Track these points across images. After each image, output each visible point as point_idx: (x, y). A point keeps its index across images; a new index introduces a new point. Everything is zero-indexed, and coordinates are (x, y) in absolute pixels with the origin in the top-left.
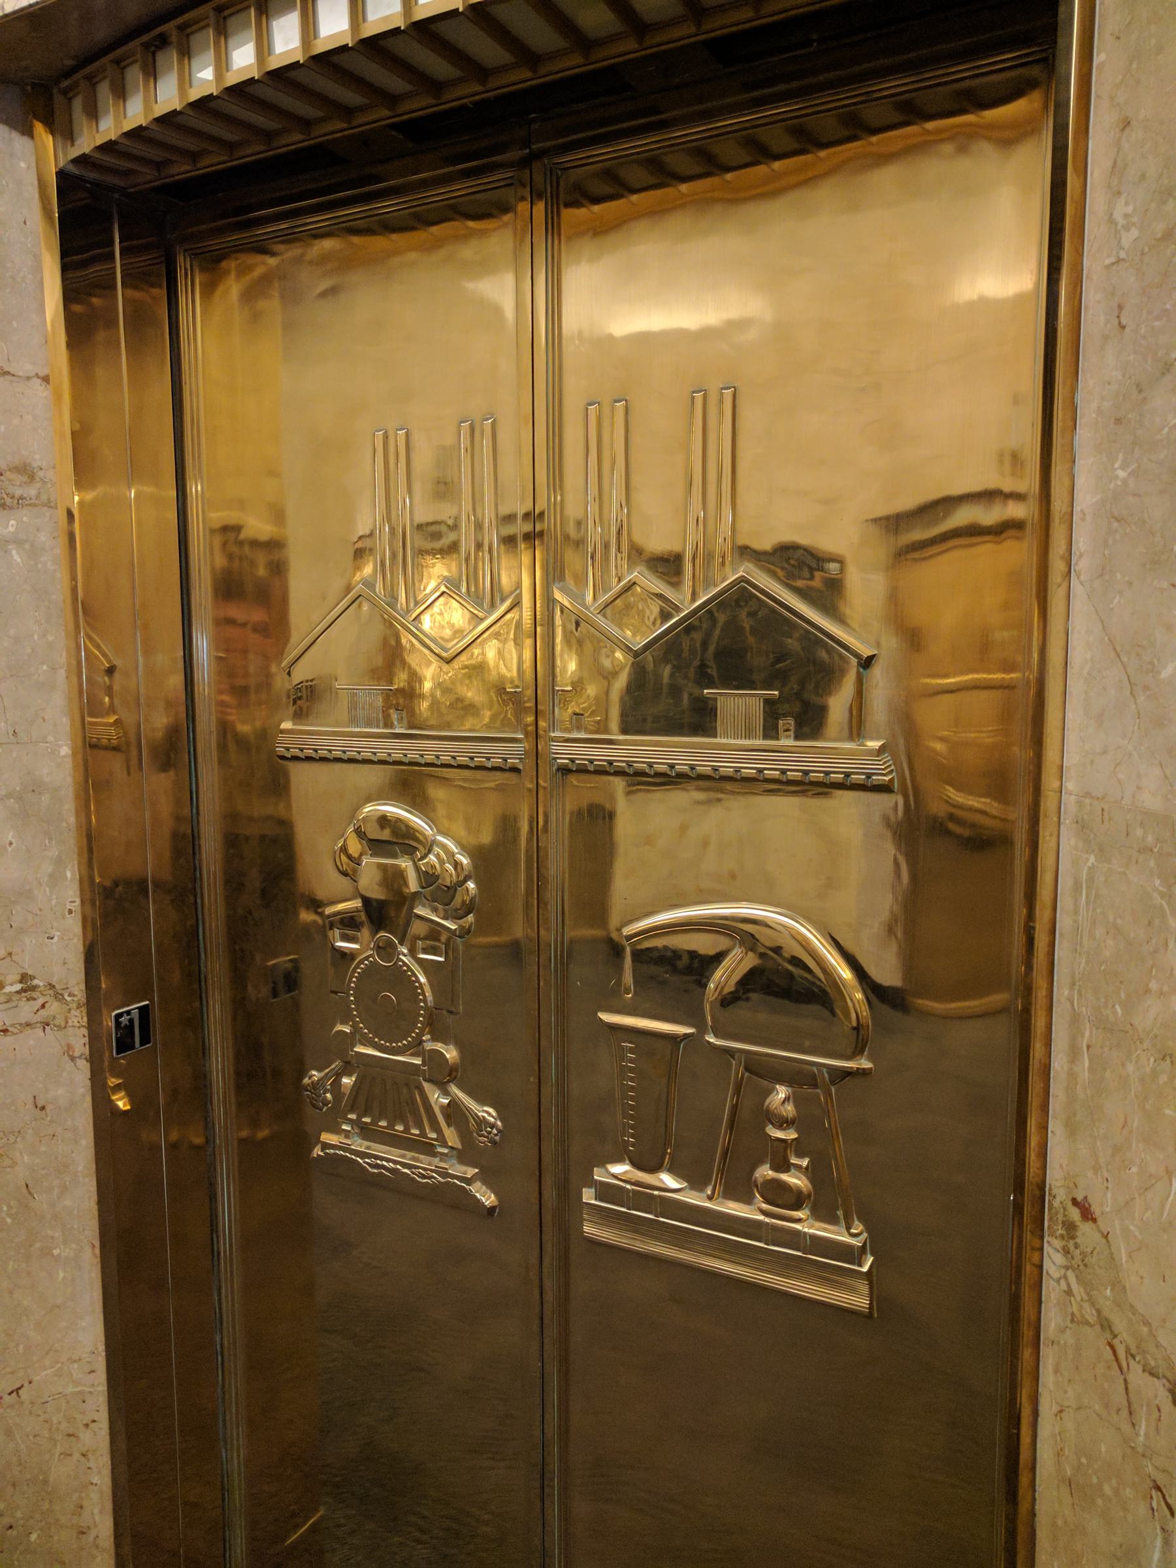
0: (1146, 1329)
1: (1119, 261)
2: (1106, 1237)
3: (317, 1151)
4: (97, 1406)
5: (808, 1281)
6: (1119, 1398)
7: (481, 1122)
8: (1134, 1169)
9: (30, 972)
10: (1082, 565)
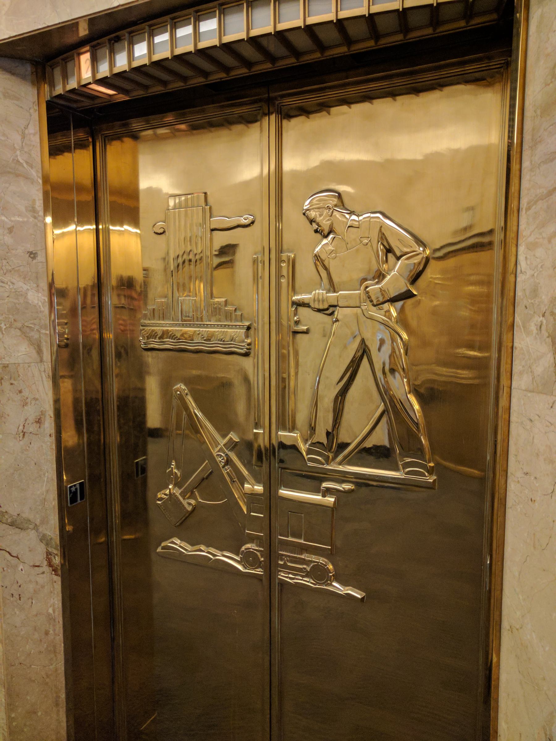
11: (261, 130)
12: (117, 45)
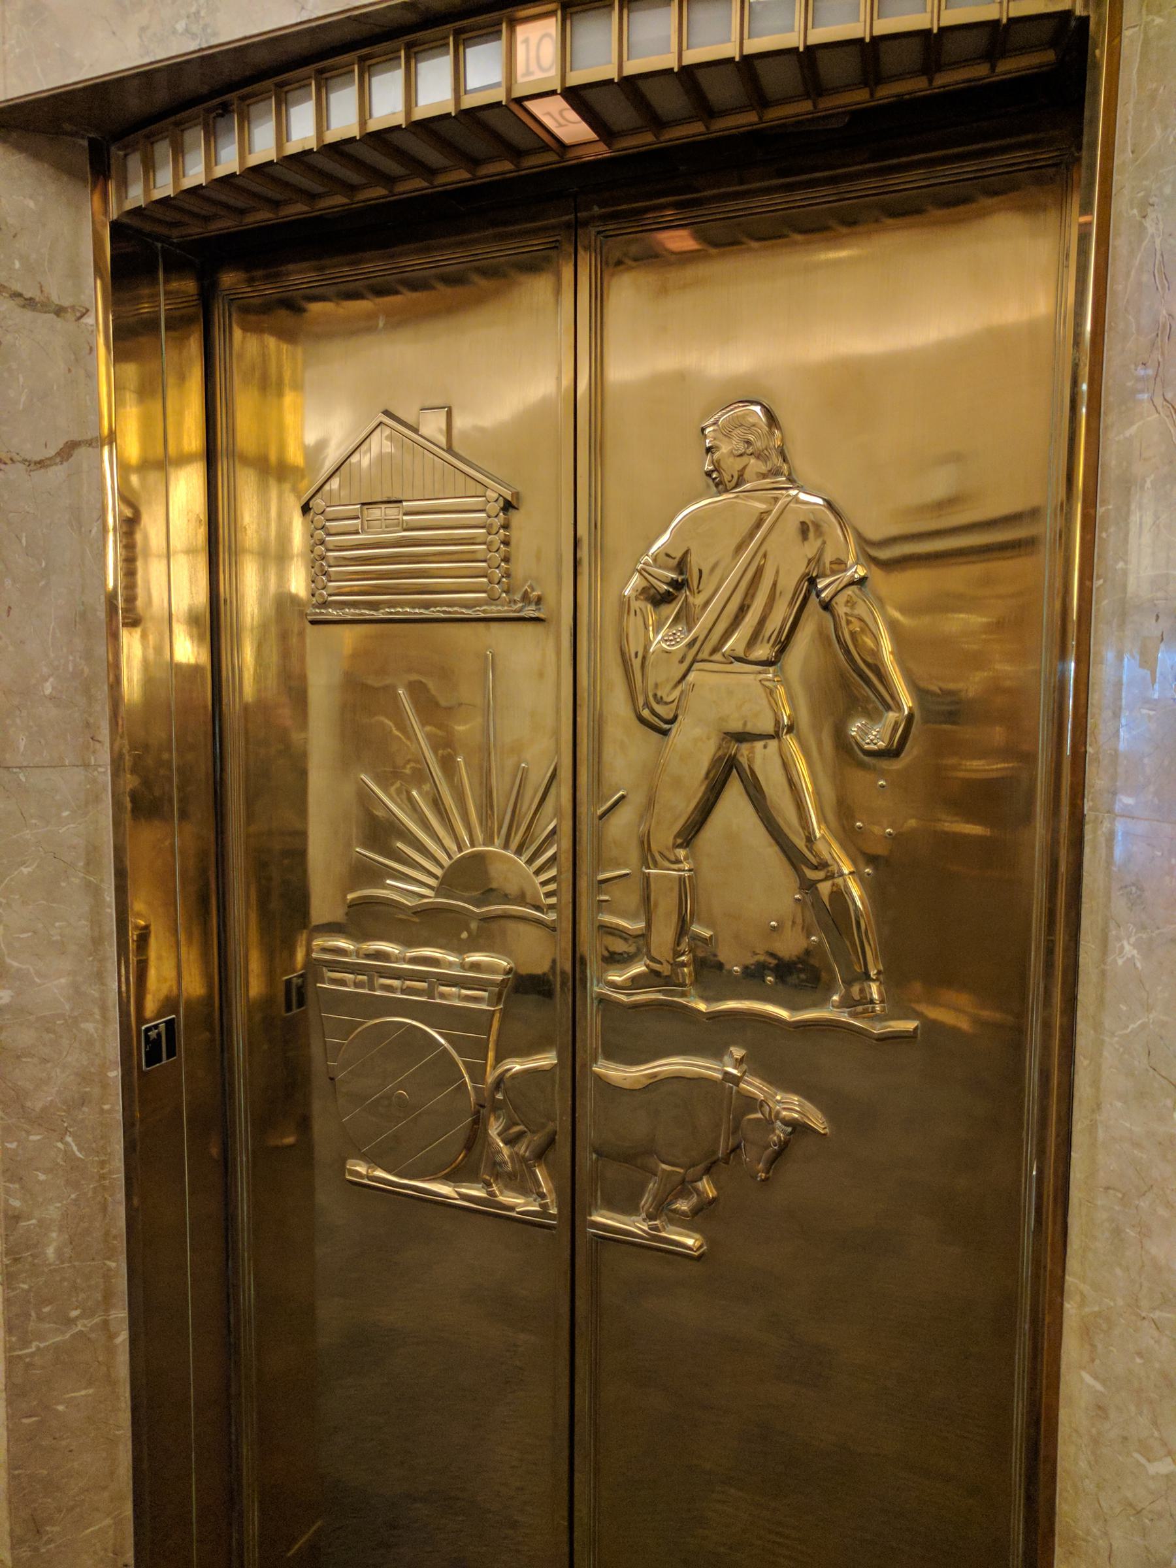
11: (558, 291)
12: (221, 123)
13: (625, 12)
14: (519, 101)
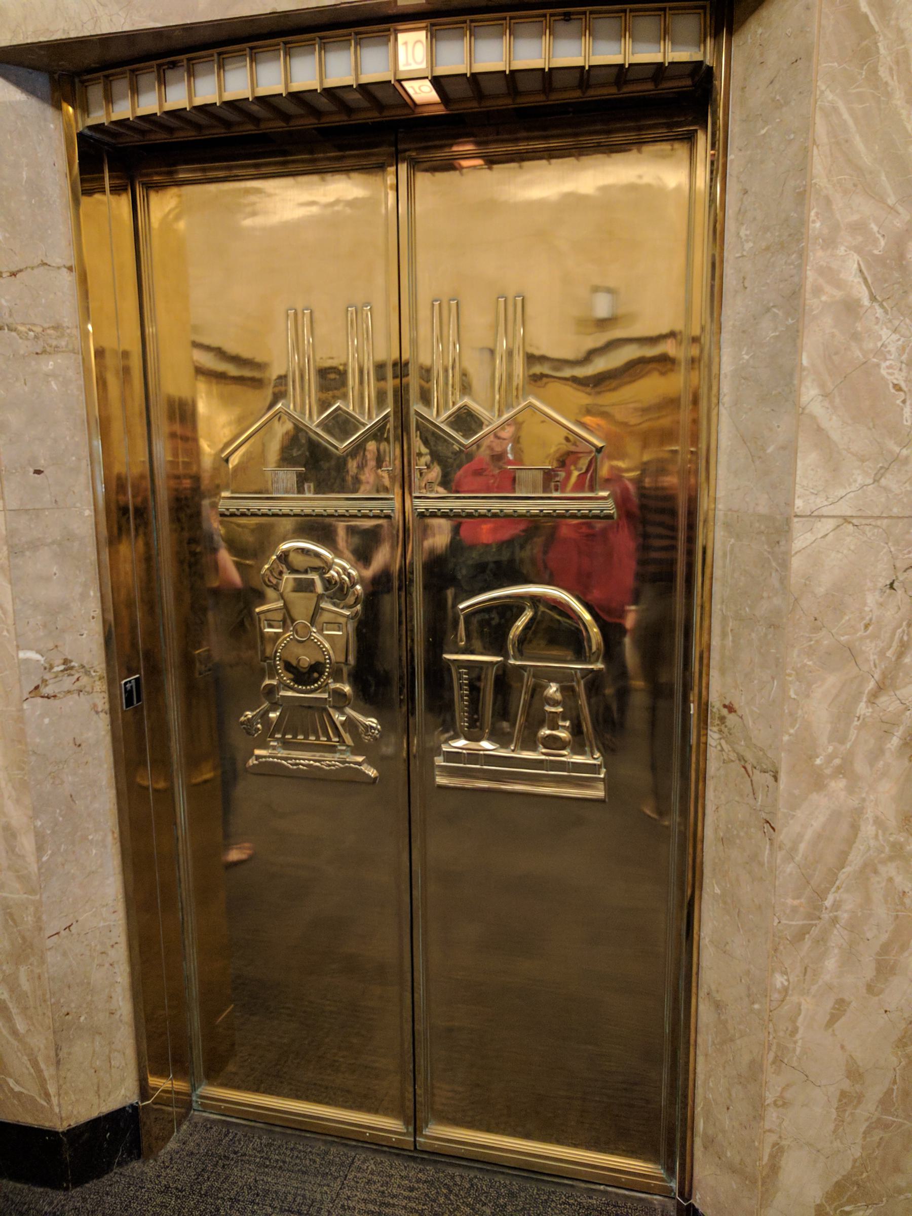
0: (761, 753)
1: (743, 256)
2: (741, 717)
3: (252, 762)
4: (119, 935)
5: (571, 788)
6: (748, 789)
7: (369, 728)
8: (756, 682)
9: (69, 658)
10: (726, 399)
12: (170, 74)
13: (434, 40)
14: (399, 81)
